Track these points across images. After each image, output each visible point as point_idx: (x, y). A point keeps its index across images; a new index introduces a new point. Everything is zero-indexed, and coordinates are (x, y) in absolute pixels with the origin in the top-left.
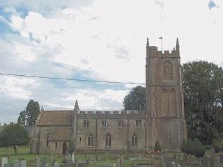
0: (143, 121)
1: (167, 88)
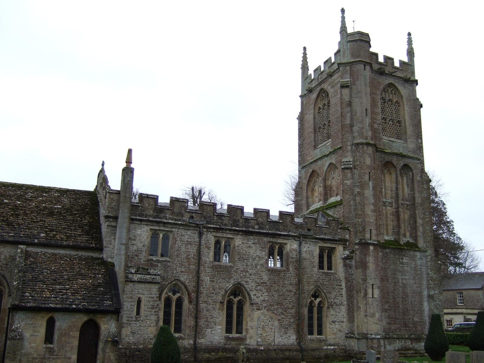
0: (340, 252)
1: (395, 160)
